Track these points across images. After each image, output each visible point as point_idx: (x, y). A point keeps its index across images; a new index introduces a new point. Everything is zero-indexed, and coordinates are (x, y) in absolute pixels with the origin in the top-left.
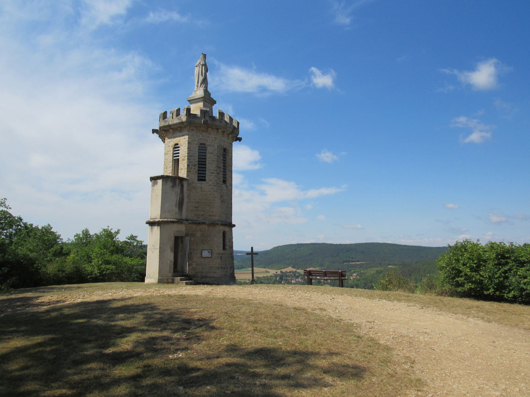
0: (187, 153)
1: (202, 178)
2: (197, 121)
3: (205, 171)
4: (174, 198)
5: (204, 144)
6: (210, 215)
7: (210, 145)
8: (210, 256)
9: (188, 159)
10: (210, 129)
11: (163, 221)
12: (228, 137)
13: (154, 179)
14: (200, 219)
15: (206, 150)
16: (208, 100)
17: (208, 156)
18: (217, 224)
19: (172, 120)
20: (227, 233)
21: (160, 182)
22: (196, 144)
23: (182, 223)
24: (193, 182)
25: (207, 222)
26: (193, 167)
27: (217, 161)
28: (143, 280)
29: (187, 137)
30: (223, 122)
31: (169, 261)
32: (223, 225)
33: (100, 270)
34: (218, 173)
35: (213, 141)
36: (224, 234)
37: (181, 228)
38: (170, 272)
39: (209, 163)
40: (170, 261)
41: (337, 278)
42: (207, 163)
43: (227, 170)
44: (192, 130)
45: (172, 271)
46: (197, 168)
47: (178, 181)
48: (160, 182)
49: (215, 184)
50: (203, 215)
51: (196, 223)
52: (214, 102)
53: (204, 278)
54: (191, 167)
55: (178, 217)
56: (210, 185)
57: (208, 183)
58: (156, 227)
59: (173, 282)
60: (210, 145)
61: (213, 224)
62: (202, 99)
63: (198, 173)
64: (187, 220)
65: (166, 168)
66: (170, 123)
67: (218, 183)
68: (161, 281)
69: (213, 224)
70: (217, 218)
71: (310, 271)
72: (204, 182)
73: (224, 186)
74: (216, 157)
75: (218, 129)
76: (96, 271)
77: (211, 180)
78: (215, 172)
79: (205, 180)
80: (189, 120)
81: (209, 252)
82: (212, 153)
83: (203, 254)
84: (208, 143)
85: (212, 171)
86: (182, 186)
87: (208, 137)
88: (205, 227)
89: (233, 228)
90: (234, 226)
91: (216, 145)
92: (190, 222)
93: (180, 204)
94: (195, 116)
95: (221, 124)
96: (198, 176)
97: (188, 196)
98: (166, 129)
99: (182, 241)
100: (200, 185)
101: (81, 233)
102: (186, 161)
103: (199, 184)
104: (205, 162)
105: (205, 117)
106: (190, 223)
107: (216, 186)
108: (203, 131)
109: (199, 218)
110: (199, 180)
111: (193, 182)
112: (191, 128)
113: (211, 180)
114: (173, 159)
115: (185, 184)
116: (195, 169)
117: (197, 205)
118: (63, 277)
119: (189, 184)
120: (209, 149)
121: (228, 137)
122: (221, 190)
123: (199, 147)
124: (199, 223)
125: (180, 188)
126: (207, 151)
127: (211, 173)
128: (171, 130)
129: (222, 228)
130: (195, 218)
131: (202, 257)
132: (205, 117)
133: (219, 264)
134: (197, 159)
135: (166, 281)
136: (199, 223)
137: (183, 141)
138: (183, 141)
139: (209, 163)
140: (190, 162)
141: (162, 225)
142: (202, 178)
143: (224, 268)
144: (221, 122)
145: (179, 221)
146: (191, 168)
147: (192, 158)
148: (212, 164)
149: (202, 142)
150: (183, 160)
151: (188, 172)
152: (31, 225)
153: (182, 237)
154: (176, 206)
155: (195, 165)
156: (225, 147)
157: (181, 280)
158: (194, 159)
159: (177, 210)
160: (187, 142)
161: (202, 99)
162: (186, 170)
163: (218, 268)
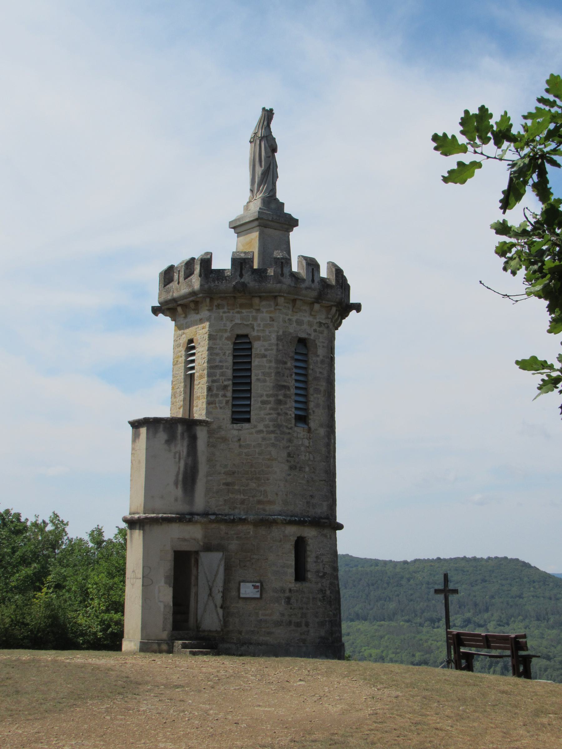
0: (206, 360)
1: (241, 416)
2: (223, 286)
3: (249, 398)
4: (172, 466)
5: (246, 336)
6: (259, 502)
7: (258, 338)
8: (258, 595)
9: (209, 375)
10: (256, 301)
11: (146, 518)
12: (312, 309)
13: (136, 425)
14: (237, 511)
15: (250, 349)
16: (274, 221)
17: (255, 362)
18: (275, 522)
19: (180, 289)
20: (310, 541)
21: (143, 431)
22: (227, 339)
23: (190, 521)
24: (220, 427)
25: (251, 517)
26: (221, 393)
27: (278, 373)
28: (118, 648)
29: (207, 324)
30: (287, 281)
31: (162, 605)
32: (291, 523)
33: (104, 624)
34: (279, 402)
35: (268, 327)
36: (300, 545)
37: (192, 534)
38: (164, 630)
39: (258, 380)
40: (165, 606)
41: (508, 652)
42: (254, 378)
43: (311, 391)
44: (218, 306)
45: (169, 626)
46: (229, 394)
47: (180, 429)
48: (143, 431)
49: (272, 429)
50: (243, 502)
51: (225, 522)
52: (292, 223)
53: (244, 644)
54: (215, 392)
55: (183, 508)
56: (261, 431)
57: (255, 426)
58: (137, 531)
59: (170, 651)
60: (258, 338)
61: (266, 522)
62: (256, 223)
63: (233, 406)
64: (206, 514)
65: (175, 397)
66: (176, 295)
67: (279, 426)
68: (146, 647)
69: (266, 522)
70: (277, 508)
71: (458, 635)
72: (246, 425)
73: (300, 431)
74: (273, 365)
75: (275, 297)
76: (96, 628)
77: (262, 420)
78: (272, 399)
79: (248, 420)
80: (206, 286)
81: (255, 587)
82: (264, 356)
83: (242, 591)
84: (255, 334)
85: (265, 398)
86: (193, 439)
87: (255, 319)
88: (250, 529)
89: (338, 532)
90: (340, 527)
91: (274, 336)
92: (213, 517)
93: (189, 479)
94: (220, 272)
95: (279, 286)
96: (233, 412)
97: (209, 460)
98: (170, 306)
99: (197, 561)
100: (235, 433)
101: (86, 538)
102: (205, 379)
103: (233, 431)
104: (250, 377)
105: (241, 276)
106: (212, 522)
107: (273, 432)
108: (242, 306)
109: (235, 508)
110: (235, 421)
111: (220, 427)
112: (216, 303)
113: (262, 420)
114: (186, 375)
115: (202, 434)
116: (224, 396)
117: (229, 480)
118: (24, 638)
119: (211, 433)
120: (258, 347)
121: (312, 309)
122: (290, 441)
123: (235, 344)
124: (233, 521)
125: (185, 443)
126: (254, 351)
127: (263, 402)
128: (179, 309)
129: (293, 531)
130: (226, 510)
131: (239, 597)
132: (241, 276)
133: (283, 615)
134: (229, 373)
135: (155, 647)
136: (233, 521)
137: (201, 332)
138: (201, 332)
139: (258, 380)
140: (213, 381)
141: (147, 528)
142: (241, 416)
143: (298, 625)
144: (280, 282)
145: (183, 518)
146: (217, 396)
147: (218, 371)
148: (265, 381)
149: (240, 332)
150: (201, 377)
151: (209, 403)
152: (18, 516)
153: (197, 553)
154: (176, 484)
155: (225, 387)
156: (303, 335)
157: (185, 646)
158: (222, 374)
159: (179, 492)
160: (206, 336)
161: (256, 223)
162: (205, 400)
163: (278, 624)
